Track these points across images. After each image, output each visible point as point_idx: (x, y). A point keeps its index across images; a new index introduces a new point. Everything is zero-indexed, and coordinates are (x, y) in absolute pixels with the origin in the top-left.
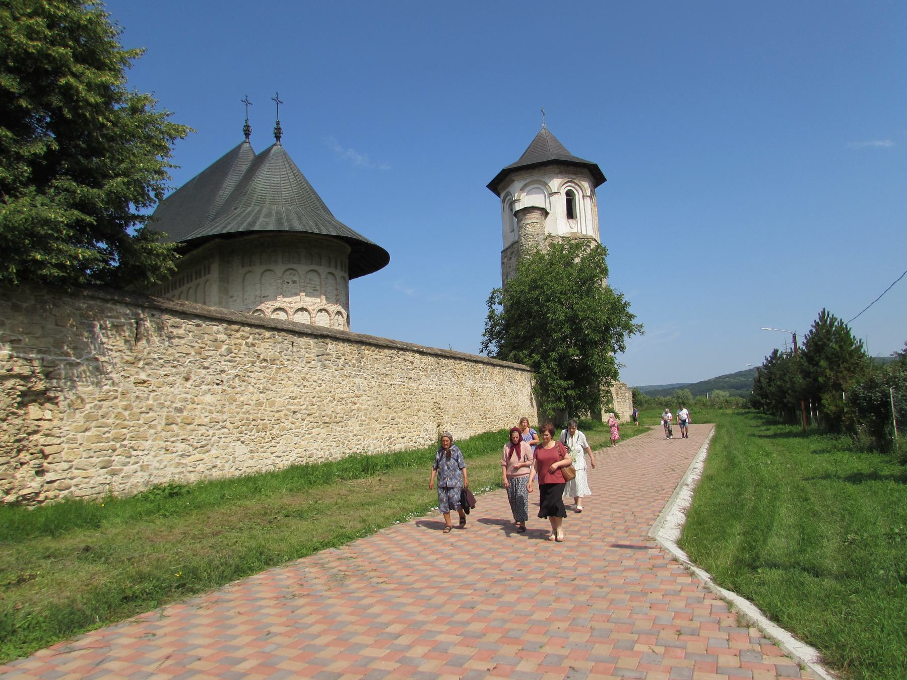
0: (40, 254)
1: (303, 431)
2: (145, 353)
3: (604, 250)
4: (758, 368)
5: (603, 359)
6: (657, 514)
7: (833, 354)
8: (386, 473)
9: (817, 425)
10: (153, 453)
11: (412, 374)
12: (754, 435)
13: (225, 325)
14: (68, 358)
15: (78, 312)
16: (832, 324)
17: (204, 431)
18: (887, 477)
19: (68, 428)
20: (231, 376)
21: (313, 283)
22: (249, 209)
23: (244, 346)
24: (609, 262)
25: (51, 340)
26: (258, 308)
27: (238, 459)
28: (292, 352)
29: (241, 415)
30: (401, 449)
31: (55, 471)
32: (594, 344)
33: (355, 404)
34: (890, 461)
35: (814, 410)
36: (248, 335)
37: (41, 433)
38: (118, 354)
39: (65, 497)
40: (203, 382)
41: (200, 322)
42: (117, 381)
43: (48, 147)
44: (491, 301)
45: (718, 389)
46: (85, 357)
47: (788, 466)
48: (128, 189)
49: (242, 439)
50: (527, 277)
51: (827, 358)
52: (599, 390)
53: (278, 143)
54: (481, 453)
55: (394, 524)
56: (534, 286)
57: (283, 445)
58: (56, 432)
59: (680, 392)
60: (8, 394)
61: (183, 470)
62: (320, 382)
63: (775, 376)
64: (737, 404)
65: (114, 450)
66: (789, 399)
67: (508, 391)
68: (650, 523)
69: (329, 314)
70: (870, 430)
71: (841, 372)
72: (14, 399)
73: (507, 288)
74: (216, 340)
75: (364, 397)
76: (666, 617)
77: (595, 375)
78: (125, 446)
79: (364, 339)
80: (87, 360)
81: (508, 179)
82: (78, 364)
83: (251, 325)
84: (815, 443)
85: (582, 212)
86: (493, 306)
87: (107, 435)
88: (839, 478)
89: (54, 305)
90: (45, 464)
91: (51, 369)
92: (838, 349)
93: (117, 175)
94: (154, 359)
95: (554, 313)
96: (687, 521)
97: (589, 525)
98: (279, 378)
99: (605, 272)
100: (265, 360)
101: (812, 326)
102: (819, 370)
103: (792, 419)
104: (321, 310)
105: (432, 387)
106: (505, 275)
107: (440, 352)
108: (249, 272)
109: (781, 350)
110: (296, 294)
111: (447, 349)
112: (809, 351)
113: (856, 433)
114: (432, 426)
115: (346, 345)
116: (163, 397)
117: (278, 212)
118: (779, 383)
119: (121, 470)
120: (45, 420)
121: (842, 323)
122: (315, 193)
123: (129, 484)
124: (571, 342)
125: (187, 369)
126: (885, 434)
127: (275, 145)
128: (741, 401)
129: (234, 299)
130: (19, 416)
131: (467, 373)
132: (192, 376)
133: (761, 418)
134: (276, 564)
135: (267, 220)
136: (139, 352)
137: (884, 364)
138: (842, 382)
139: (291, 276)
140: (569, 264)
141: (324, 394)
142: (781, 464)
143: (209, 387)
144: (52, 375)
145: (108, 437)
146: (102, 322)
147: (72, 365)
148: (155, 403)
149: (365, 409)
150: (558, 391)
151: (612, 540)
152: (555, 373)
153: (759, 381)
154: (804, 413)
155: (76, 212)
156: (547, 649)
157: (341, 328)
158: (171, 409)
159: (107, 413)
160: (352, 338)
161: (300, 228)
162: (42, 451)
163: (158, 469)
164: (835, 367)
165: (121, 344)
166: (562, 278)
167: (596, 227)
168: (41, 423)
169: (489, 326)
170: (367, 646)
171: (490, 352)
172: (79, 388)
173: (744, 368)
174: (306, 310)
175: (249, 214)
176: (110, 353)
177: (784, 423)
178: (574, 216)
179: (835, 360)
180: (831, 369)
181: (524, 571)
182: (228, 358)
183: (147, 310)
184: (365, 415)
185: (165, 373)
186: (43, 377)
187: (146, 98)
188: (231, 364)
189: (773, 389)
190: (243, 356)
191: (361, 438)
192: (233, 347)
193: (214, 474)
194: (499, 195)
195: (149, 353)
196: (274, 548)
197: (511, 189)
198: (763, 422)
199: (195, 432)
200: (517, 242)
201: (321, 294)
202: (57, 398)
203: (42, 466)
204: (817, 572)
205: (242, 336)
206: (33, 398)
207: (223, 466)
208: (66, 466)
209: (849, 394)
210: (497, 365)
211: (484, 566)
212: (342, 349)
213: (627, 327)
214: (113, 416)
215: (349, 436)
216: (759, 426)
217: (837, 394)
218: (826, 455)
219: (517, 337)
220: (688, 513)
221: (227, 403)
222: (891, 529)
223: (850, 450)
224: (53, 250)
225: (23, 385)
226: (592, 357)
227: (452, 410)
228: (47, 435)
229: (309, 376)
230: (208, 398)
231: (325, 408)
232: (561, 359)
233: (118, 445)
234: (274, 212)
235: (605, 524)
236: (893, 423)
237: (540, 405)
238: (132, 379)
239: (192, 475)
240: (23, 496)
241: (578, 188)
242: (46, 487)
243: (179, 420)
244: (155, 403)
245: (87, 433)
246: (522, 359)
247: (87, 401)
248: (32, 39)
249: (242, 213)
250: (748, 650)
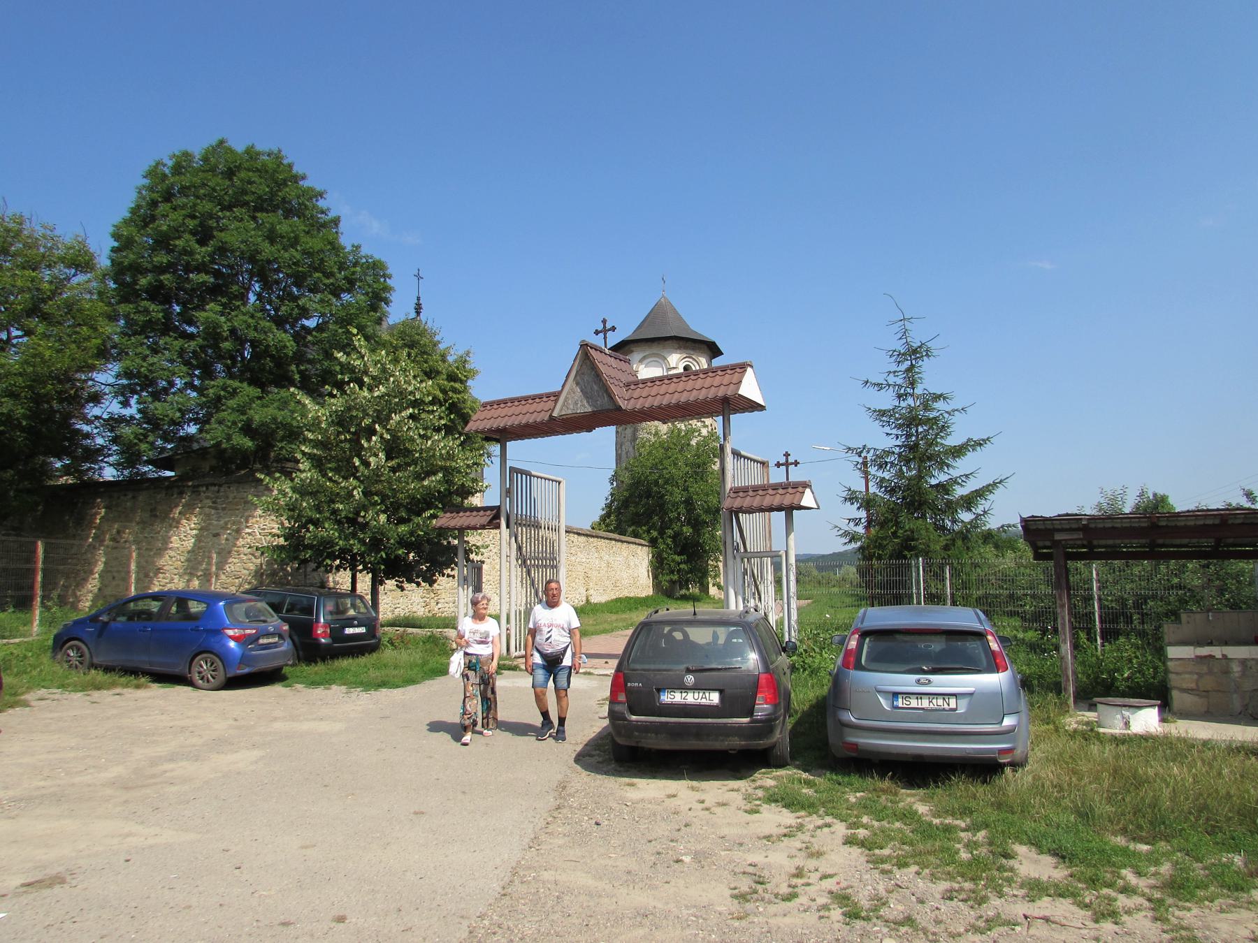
52: (708, 565)
67: (632, 564)
77: (705, 551)
81: (627, 348)
105: (584, 560)
114: (582, 590)
152: (671, 549)
210: (625, 542)
232: (675, 537)
237: (655, 577)
241: (696, 364)
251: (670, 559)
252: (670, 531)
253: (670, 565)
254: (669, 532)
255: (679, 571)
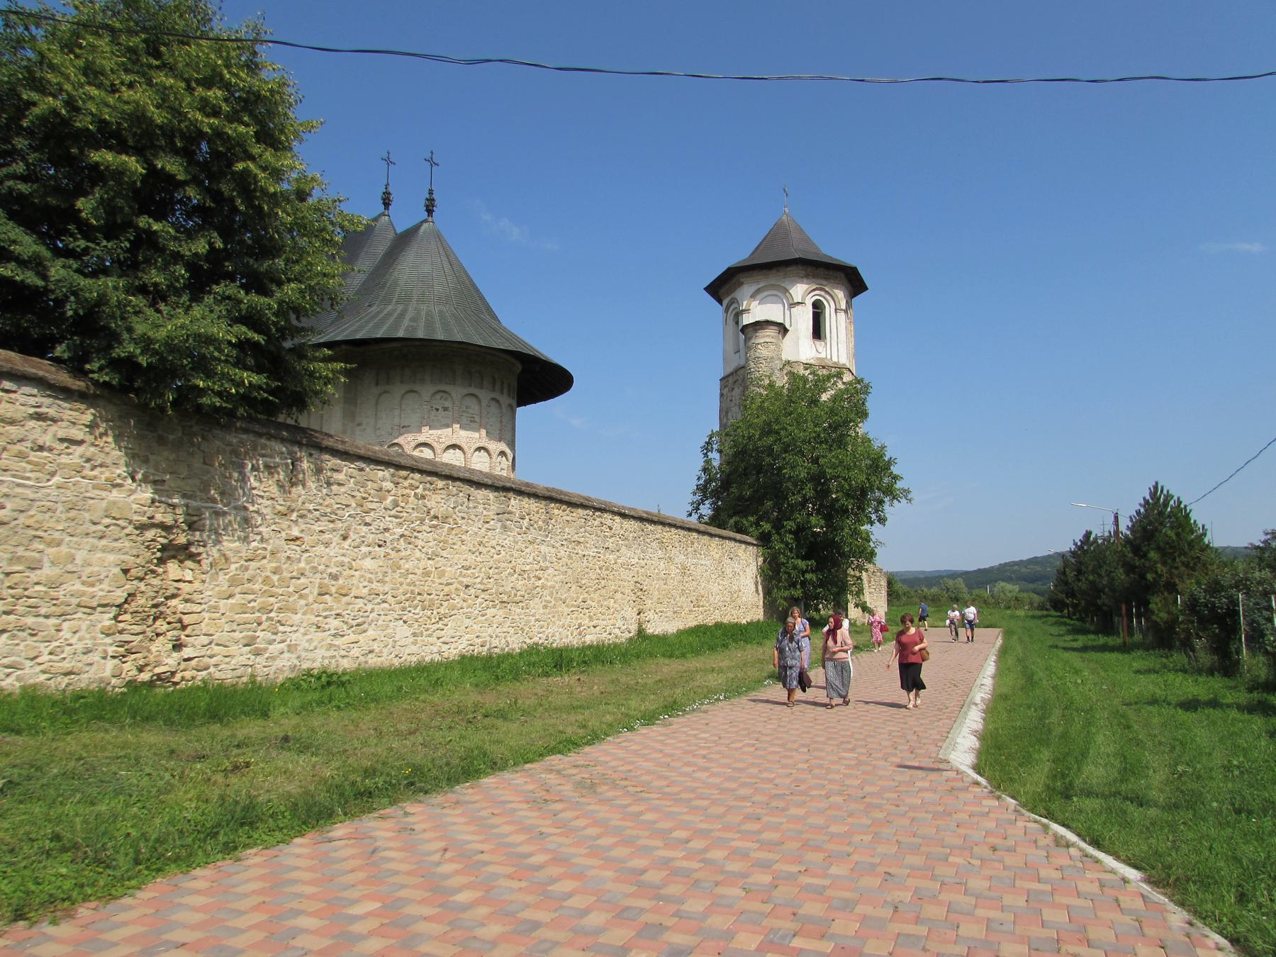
0: (201, 379)
1: (476, 612)
2: (300, 503)
3: (867, 386)
4: (1063, 556)
5: (856, 533)
6: (945, 735)
7: (1168, 543)
8: (584, 671)
9: (1141, 637)
10: (302, 630)
11: (610, 543)
12: (1056, 647)
13: (392, 470)
14: (214, 505)
15: (228, 449)
16: (1166, 504)
17: (362, 605)
18: (1229, 706)
19: (209, 593)
20: (396, 537)
21: (471, 411)
22: (390, 308)
23: (412, 499)
24: (871, 405)
25: (197, 482)
26: (396, 441)
27: (399, 643)
28: (468, 508)
29: (404, 586)
30: (592, 642)
31: (193, 646)
32: (844, 511)
33: (540, 579)
34: (1236, 687)
35: (1139, 617)
36: (418, 484)
37: (181, 598)
38: (269, 502)
39: (203, 680)
40: (363, 542)
41: (363, 465)
42: (266, 536)
43: (211, 244)
44: (707, 447)
45: (1003, 580)
46: (233, 504)
47: (1104, 687)
48: (304, 297)
49: (405, 618)
50: (758, 417)
51: (1158, 549)
52: (847, 575)
53: (430, 219)
54: (697, 652)
55: (620, 732)
56: (767, 430)
57: (451, 628)
58: (196, 597)
59: (950, 583)
60: (148, 547)
61: (335, 653)
62: (498, 548)
63: (1087, 568)
64: (1031, 604)
65: (259, 624)
66: (1104, 600)
67: (728, 571)
68: (939, 744)
69: (489, 455)
70: (1211, 647)
71: (1177, 568)
72: (154, 553)
73: (726, 430)
74: (381, 489)
75: (551, 571)
76: (977, 835)
77: (843, 555)
78: (271, 619)
79: (554, 494)
80: (235, 508)
81: (734, 280)
82: (225, 513)
83: (421, 472)
84: (1138, 660)
85: (834, 330)
86: (709, 454)
87: (253, 604)
88: (1169, 704)
89: (203, 438)
90: (183, 637)
91: (195, 518)
92: (1174, 537)
93: (289, 280)
94: (309, 511)
95: (793, 468)
96: (982, 745)
97: (864, 743)
98: (450, 542)
99: (864, 415)
100: (436, 517)
101: (1140, 505)
102: (1147, 565)
103: (1107, 627)
104: (479, 449)
105: (634, 561)
106: (724, 412)
107: (645, 515)
108: (386, 392)
109: (1097, 532)
110: (448, 426)
111: (655, 511)
112: (1135, 538)
113: (1193, 650)
114: (631, 613)
115: (532, 501)
116: (317, 559)
117: (429, 314)
118: (1091, 578)
119: (266, 649)
120: (184, 582)
121: (1180, 503)
122: (477, 290)
123: (274, 668)
124: (813, 508)
125: (346, 524)
126: (1231, 652)
127: (425, 221)
128: (1037, 599)
129: (363, 427)
130: (158, 575)
131: (677, 545)
132: (351, 533)
133: (1065, 624)
134: (501, 769)
135: (414, 324)
136: (293, 501)
137: (1235, 558)
138: (1177, 581)
139: (442, 401)
140: (814, 402)
141: (503, 565)
142: (1095, 684)
143: (370, 548)
144: (195, 526)
145: (253, 607)
146: (254, 462)
147: (218, 514)
148: (308, 567)
149: (551, 587)
150: (794, 573)
151: (898, 760)
152: (791, 550)
153: (1064, 573)
154: (1125, 619)
155: (244, 329)
156: (855, 857)
157: (504, 473)
158: (325, 575)
159: (254, 577)
160: (540, 492)
161: (459, 337)
162: (180, 621)
163: (307, 650)
164: (1169, 561)
165: (274, 490)
166: (806, 422)
167: (852, 351)
168: (181, 585)
169: (701, 482)
170: (658, 848)
171: (701, 517)
172: (225, 543)
173: (1040, 553)
174: (460, 448)
175: (390, 314)
176: (260, 501)
177: (1096, 633)
178: (822, 335)
179: (1169, 552)
180: (1164, 563)
181: (802, 787)
182: (393, 512)
183: (304, 448)
184: (551, 594)
185: (320, 529)
186: (186, 528)
187: (313, 179)
188: (397, 520)
189: (1083, 585)
190: (410, 511)
191: (545, 624)
192: (400, 499)
193: (370, 661)
194: (720, 302)
195: (304, 503)
196: (497, 751)
197: (738, 294)
198: (1068, 631)
199: (351, 606)
200: (743, 367)
201: (481, 426)
202: (199, 554)
203: (179, 639)
204: (1140, 802)
205: (411, 485)
206: (172, 553)
207: (381, 652)
208: (205, 640)
209: (1186, 597)
210: (715, 536)
211: (754, 780)
212: (527, 506)
213: (890, 492)
214: (260, 580)
215: (530, 621)
216: (1062, 635)
217: (1170, 598)
218: (1153, 676)
219: (740, 498)
220: (982, 737)
221: (390, 571)
222: (1229, 761)
223: (1184, 671)
224: (216, 374)
225: (165, 537)
226: (843, 529)
227: (657, 593)
228: (187, 601)
229: (486, 540)
230: (368, 563)
231: (504, 583)
232: (799, 532)
233: (264, 617)
234: (423, 313)
235: (885, 743)
236: (1240, 638)
237: (768, 593)
238: (283, 534)
239: (345, 660)
240: (158, 675)
241: (829, 298)
242: (183, 665)
243: (333, 590)
244: (308, 567)
245: (231, 601)
246: (746, 529)
247: (233, 560)
248: (208, 116)
249: (379, 312)
250: (1069, 866)
251: (790, 565)
252: (791, 523)
253: (789, 574)
254: (790, 525)
255: (803, 584)
